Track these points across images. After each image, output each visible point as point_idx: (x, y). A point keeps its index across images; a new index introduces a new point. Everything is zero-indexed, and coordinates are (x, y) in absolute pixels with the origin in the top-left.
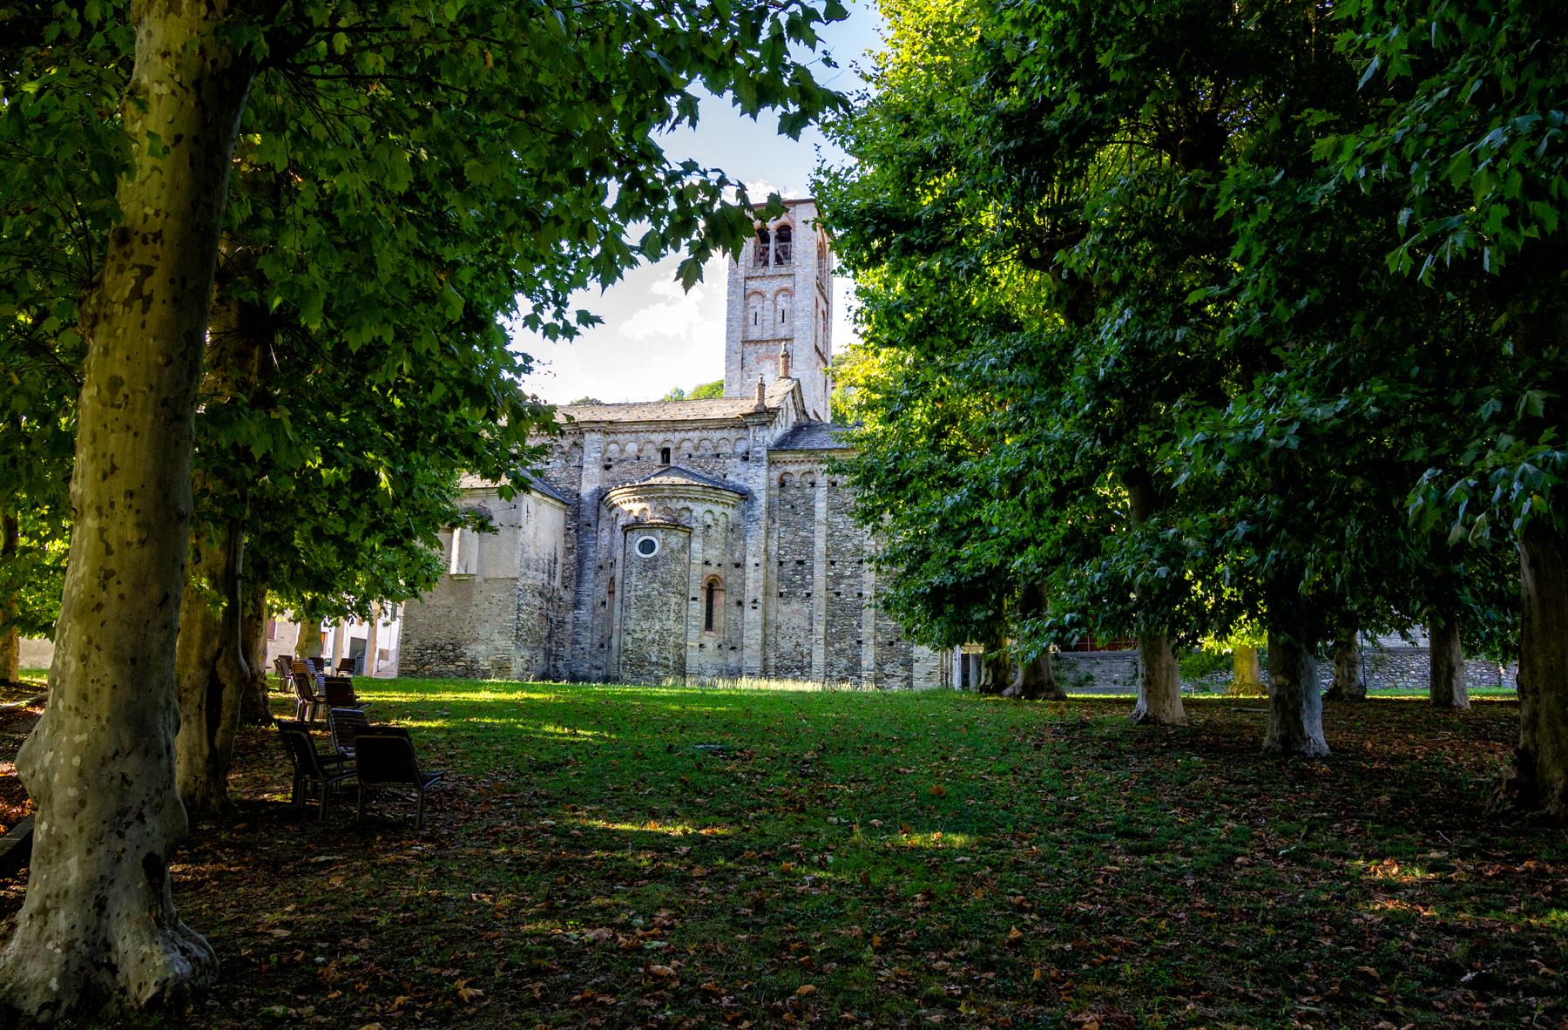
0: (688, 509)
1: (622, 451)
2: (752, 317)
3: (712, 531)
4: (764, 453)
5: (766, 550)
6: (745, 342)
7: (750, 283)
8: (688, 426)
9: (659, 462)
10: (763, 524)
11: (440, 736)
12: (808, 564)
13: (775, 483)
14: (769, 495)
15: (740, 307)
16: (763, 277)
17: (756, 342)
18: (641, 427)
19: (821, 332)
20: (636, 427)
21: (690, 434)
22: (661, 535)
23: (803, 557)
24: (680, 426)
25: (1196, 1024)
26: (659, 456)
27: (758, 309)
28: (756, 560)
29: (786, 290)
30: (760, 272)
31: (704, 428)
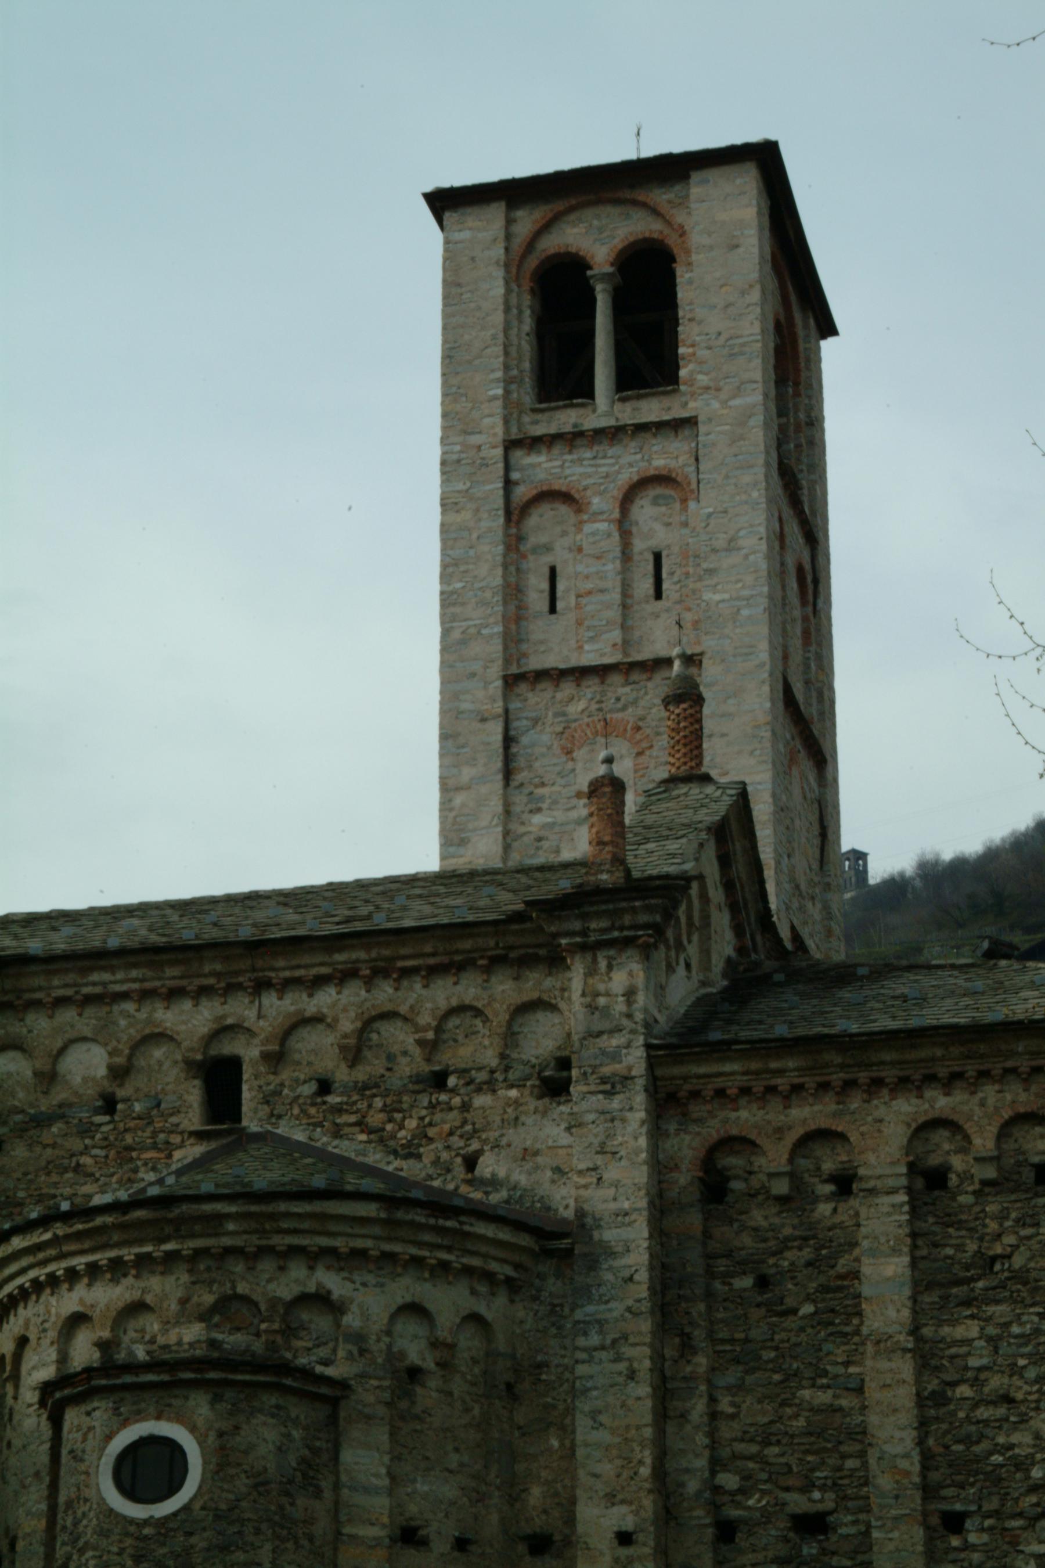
0: (321, 1300)
1: (48, 1078)
2: (537, 585)
3: (427, 1395)
4: (635, 1059)
5: (660, 1473)
6: (511, 681)
7: (523, 459)
8: (315, 964)
9: (193, 1119)
10: (641, 1356)
11: (146, 1531)
12: (846, 1526)
13: (684, 1178)
14: (659, 1232)
15: (492, 550)
16: (573, 438)
17: (558, 676)
18: (117, 979)
19: (796, 643)
20: (99, 978)
21: (325, 999)
22: (200, 1405)
23: (819, 1500)
24: (281, 967)
25: (115, 1565)
26: (194, 1094)
27: (560, 556)
28: (622, 1517)
29: (663, 479)
30: (566, 419)
31: (380, 972)
